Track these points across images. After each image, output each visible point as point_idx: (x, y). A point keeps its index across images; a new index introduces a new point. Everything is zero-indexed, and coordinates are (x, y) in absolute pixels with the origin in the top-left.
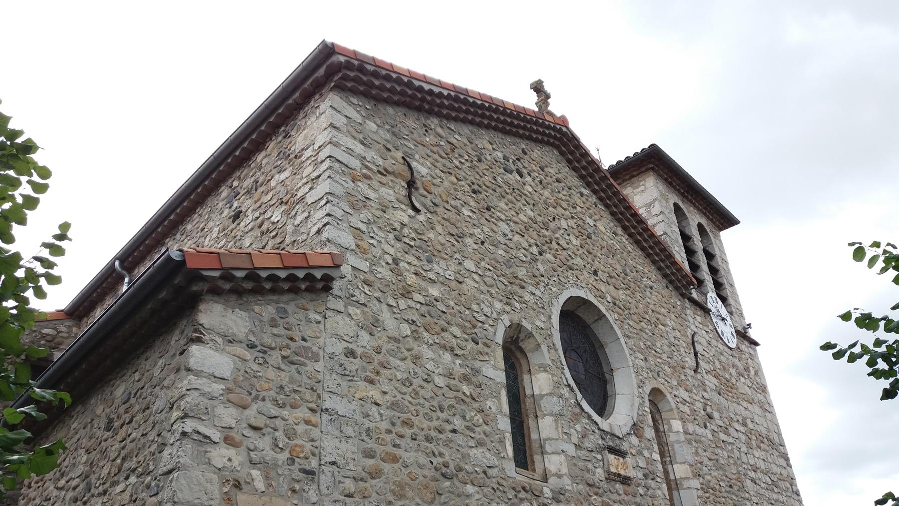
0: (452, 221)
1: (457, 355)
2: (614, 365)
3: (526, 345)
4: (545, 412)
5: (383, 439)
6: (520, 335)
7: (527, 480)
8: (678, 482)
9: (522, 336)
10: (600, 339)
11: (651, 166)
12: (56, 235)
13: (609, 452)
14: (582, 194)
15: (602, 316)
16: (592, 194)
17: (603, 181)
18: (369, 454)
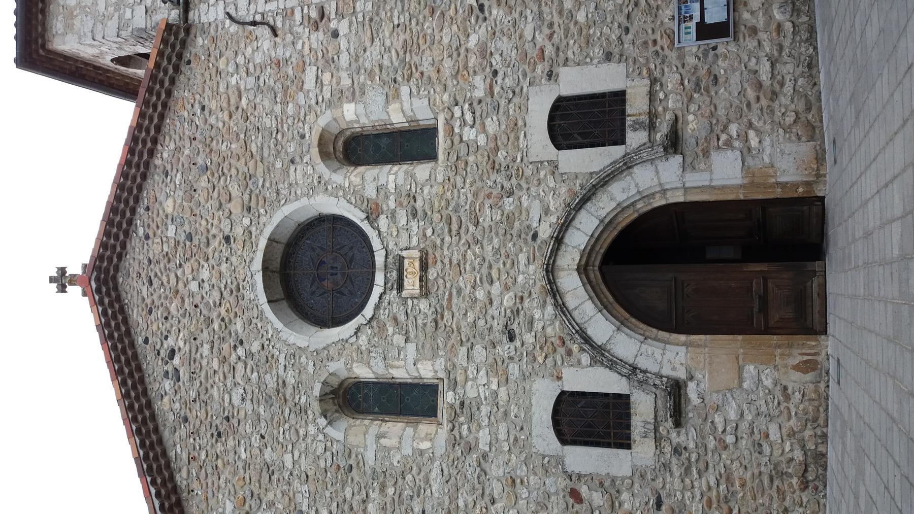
1: (367, 496)
2: (317, 214)
6: (328, 392)
9: (328, 390)
10: (294, 229)
12: (624, 102)
15: (271, 240)
16: (137, 214)
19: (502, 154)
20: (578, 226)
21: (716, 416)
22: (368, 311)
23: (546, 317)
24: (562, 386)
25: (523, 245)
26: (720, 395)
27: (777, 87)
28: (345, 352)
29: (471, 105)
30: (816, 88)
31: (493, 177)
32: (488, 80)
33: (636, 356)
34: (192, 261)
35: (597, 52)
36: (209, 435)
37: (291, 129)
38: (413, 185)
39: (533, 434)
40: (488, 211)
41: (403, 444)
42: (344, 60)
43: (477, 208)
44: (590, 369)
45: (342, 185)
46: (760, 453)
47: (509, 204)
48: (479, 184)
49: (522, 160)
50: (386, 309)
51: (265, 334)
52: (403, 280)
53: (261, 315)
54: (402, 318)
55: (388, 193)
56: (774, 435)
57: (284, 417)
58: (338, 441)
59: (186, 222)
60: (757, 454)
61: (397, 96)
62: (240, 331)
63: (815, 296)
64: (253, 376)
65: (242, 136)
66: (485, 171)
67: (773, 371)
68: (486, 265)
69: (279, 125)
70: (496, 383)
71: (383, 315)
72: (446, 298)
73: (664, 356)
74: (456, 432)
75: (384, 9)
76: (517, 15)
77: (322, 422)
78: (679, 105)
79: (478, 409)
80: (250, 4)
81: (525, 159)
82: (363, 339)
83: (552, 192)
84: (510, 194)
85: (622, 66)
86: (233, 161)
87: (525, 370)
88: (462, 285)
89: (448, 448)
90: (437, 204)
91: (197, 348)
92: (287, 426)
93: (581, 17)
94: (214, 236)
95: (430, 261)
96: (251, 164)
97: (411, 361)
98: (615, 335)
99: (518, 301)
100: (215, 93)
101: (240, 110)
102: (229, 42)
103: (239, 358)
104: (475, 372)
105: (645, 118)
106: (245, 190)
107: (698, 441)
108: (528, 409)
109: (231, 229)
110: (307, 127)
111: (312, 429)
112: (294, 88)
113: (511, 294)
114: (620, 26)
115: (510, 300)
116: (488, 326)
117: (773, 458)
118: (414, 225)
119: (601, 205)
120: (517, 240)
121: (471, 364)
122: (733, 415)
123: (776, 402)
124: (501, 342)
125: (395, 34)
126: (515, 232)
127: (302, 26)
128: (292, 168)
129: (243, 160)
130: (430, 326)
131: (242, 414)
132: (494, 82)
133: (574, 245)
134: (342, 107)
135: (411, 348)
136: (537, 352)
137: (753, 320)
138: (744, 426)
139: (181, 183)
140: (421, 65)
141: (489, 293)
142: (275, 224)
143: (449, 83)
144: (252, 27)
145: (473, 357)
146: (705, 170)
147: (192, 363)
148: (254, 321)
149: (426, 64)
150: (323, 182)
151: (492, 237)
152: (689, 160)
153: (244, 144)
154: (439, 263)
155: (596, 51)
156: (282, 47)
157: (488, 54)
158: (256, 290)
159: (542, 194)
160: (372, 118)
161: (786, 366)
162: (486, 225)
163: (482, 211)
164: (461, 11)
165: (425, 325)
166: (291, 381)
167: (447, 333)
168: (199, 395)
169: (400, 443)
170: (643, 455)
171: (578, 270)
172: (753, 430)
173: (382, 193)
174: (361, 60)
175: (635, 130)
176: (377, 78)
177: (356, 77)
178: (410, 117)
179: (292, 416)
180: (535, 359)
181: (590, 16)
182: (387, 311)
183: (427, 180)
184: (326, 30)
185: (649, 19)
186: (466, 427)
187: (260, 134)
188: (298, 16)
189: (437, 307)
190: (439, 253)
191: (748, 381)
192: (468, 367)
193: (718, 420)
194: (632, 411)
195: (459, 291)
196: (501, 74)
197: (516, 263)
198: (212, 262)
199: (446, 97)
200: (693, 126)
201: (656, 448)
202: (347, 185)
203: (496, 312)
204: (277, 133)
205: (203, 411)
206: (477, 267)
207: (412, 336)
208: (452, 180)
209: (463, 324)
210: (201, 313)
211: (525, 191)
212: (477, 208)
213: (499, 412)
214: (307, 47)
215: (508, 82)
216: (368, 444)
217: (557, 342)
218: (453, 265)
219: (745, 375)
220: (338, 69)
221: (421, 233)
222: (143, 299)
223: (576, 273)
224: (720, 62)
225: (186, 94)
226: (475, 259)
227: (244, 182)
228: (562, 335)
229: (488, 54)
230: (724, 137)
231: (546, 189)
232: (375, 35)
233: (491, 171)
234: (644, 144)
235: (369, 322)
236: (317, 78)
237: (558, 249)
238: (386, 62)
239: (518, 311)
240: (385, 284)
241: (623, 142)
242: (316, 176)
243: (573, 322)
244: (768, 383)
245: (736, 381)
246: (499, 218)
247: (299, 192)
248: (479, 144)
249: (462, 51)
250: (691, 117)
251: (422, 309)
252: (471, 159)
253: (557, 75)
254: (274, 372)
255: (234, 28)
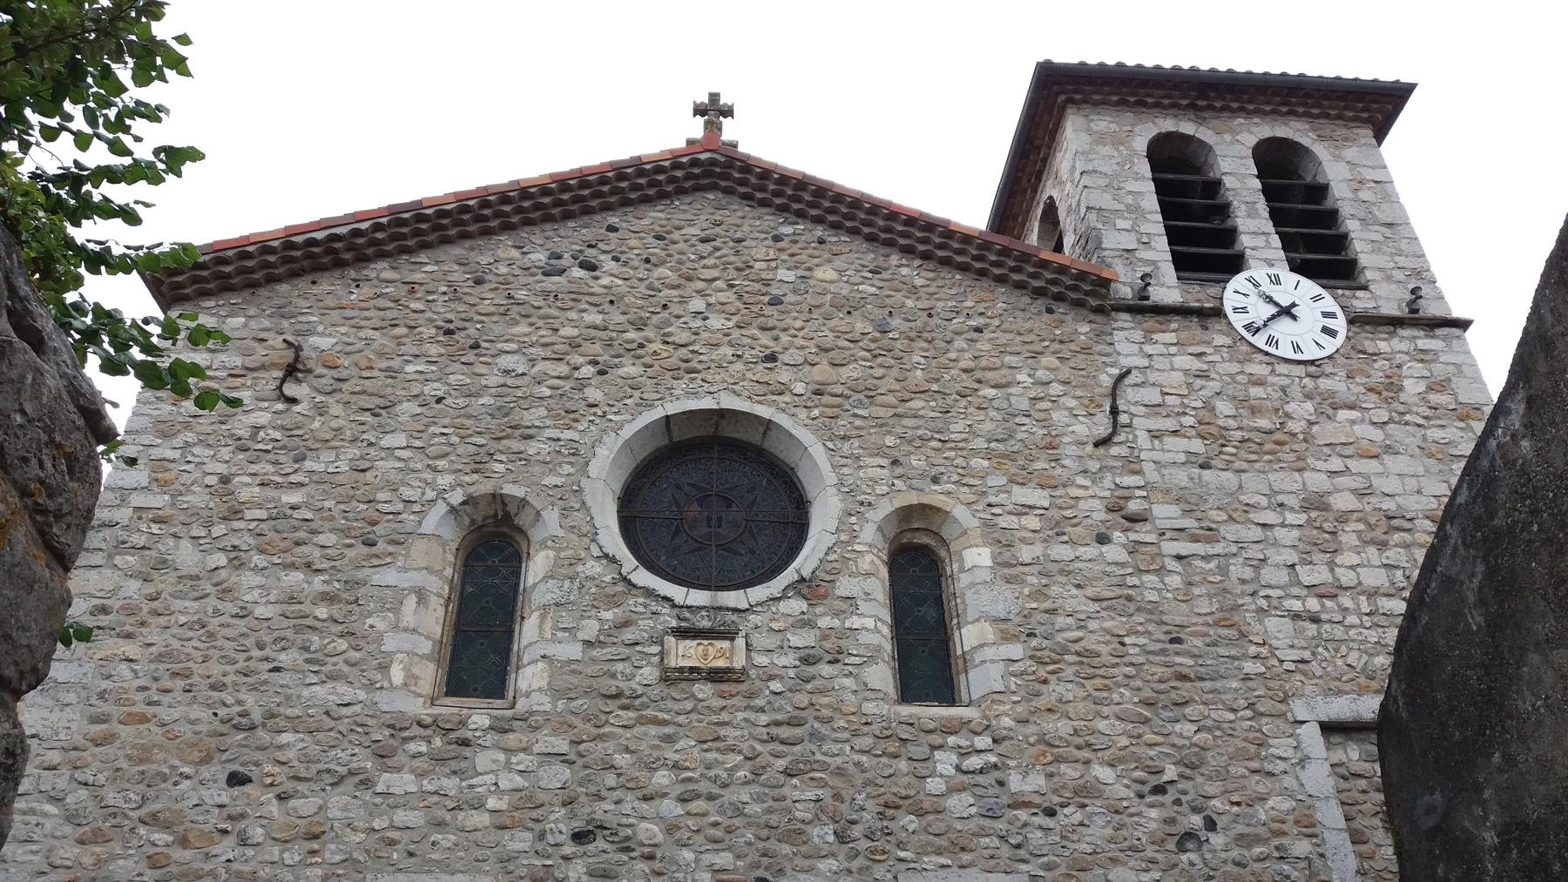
0: (370, 390)
2: (810, 497)
3: (524, 520)
5: (127, 699)
6: (508, 508)
7: (456, 710)
8: (968, 657)
9: (512, 509)
11: (1062, 98)
15: (768, 425)
17: (822, 197)
18: (97, 720)
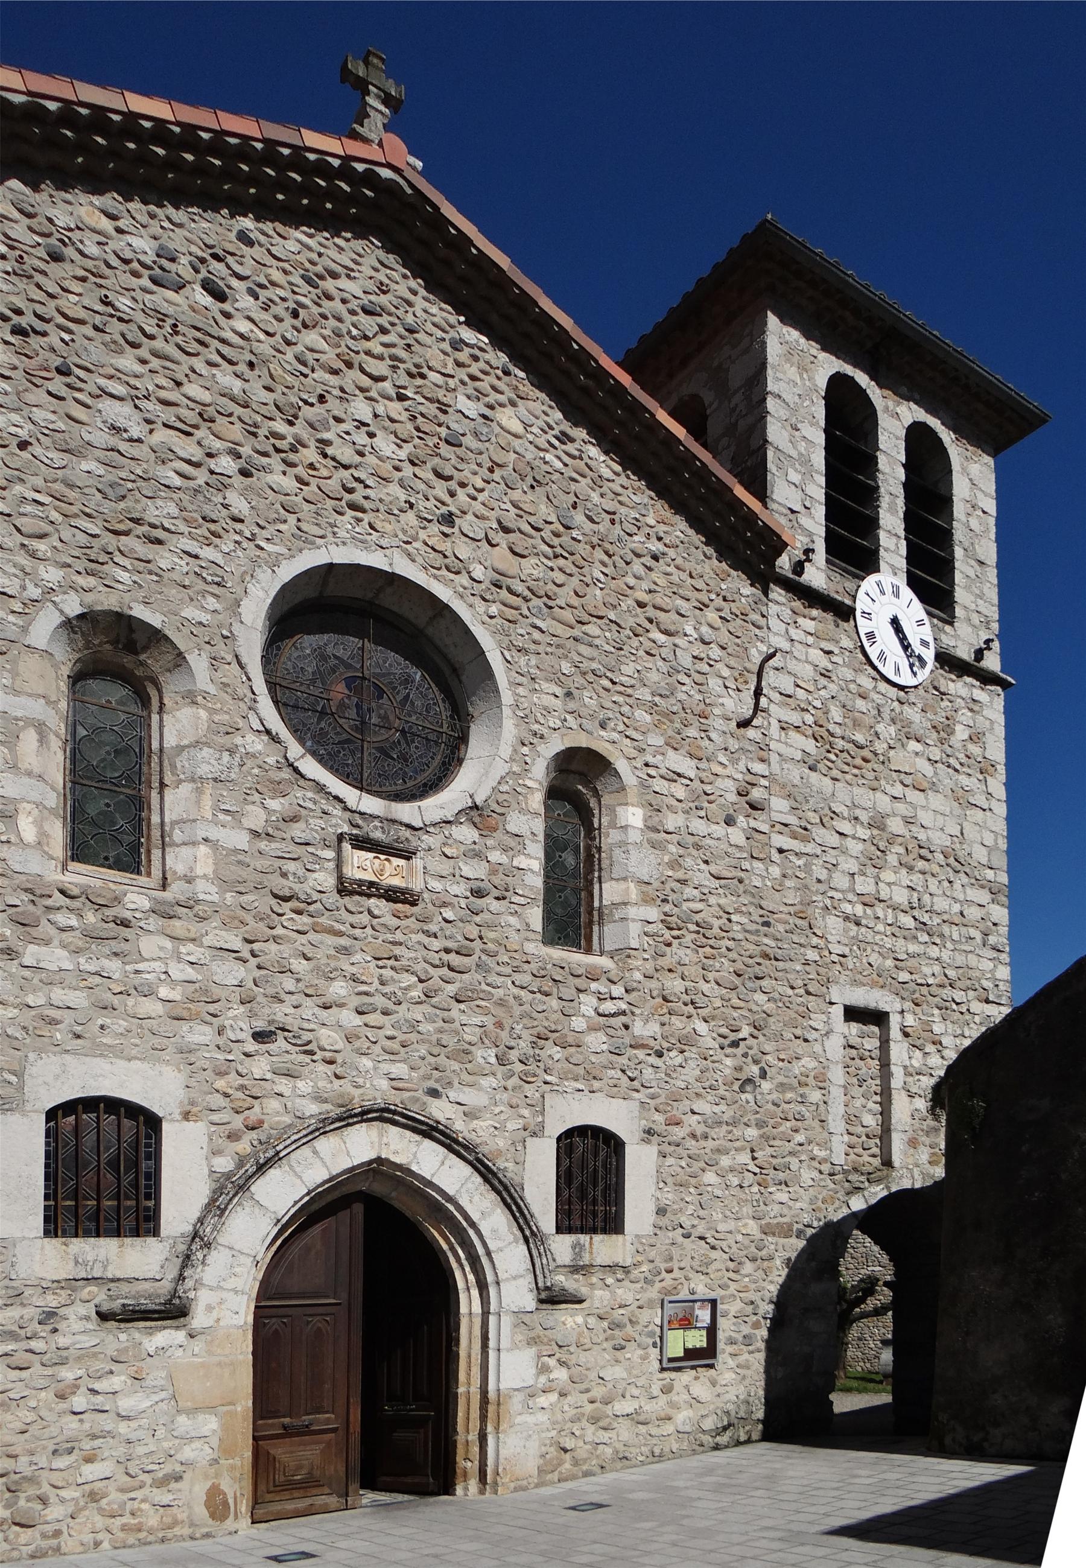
4: (182, 776)
13: (354, 847)
14: (457, 345)
19: (557, 1052)
20: (447, 1163)
21: (123, 1378)
22: (311, 767)
23: (298, 1100)
24: (172, 1120)
25: (422, 1072)
26: (163, 1382)
27: (603, 1423)
28: (228, 698)
29: (624, 1013)
30: (598, 1470)
31: (526, 1034)
32: (652, 1043)
33: (231, 1248)
34: (410, 426)
35: (668, 1196)
36: (21, 304)
37: (616, 708)
38: (522, 901)
39: (68, 1058)
40: (477, 1020)
41: (26, 780)
42: (699, 826)
43: (483, 1003)
44: (206, 1171)
45: (529, 775)
46: (55, 1452)
47: (486, 1055)
48: (517, 1011)
49: (546, 1083)
50: (315, 803)
51: (266, 534)
52: (370, 850)
53: (303, 539)
54: (298, 831)
55: (511, 853)
56: (90, 1471)
57: (76, 516)
58: (25, 630)
59: (480, 445)
60: (52, 1448)
61: (647, 900)
62: (270, 479)
63: (308, 1501)
64: (172, 474)
65: (612, 616)
66: (536, 1023)
67: (208, 1458)
68: (390, 1006)
69: (622, 689)
70: (171, 997)
71: (302, 795)
72: (335, 924)
73: (232, 1293)
74: (58, 899)
75: (751, 903)
76: (721, 1092)
77: (73, 606)
78: (597, 1304)
79: (116, 954)
80: (781, 694)
81: (547, 1087)
82: (257, 744)
83: (498, 1126)
84: (501, 1060)
85: (650, 1230)
86: (574, 582)
87: (199, 1053)
88: (358, 957)
89: (23, 878)
90: (492, 935)
91: (231, 362)
92: (55, 516)
93: (710, 1177)
94: (452, 494)
95: (399, 906)
96: (567, 615)
97: (214, 833)
98: (269, 1214)
99: (328, 1055)
100: (675, 590)
101: (647, 625)
102: (737, 640)
103: (210, 455)
104: (192, 959)
105: (586, 1260)
106: (528, 588)
107: (71, 1351)
108: (118, 1052)
109: (466, 536)
110: (615, 736)
111: (52, 575)
112: (670, 733)
113: (340, 1045)
114: (693, 1226)
115: (330, 1040)
116: (283, 996)
117: (45, 1474)
118: (460, 889)
119: (476, 1198)
120: (430, 1064)
121: (208, 952)
122: (125, 1404)
123: (150, 1467)
124: (252, 1015)
125: (722, 913)
126: (442, 1060)
127: (745, 770)
128: (559, 691)
129: (575, 601)
130: (284, 886)
131: (79, 413)
132: (650, 1052)
133: (418, 1155)
134: (637, 806)
135: (240, 840)
136: (233, 1079)
137: (270, 1418)
138: (106, 1422)
139: (546, 463)
140: (680, 944)
141: (341, 1005)
142: (472, 628)
143: (653, 984)
144: (753, 689)
145: (222, 959)
146: (513, 1341)
147: (199, 335)
148: (292, 519)
149: (681, 952)
150: (535, 741)
151: (435, 1022)
152: (527, 1318)
153: (600, 614)
154: (395, 922)
155: (670, 1196)
156: (724, 729)
157: (683, 1047)
158: (356, 547)
159: (497, 1110)
160: (617, 852)
161: (217, 1475)
162: (454, 1013)
163: (477, 1010)
164: (735, 1015)
165: (284, 875)
166: (164, 559)
167: (269, 916)
168: (120, 319)
169: (29, 774)
170: (37, 1258)
171: (379, 1160)
172: (100, 1437)
173: (512, 842)
174: (694, 852)
175: (574, 1247)
176: (670, 873)
177: (674, 838)
178: (611, 914)
179: (82, 539)
180: (221, 1074)
181: (709, 1189)
182: (310, 805)
183: (527, 925)
184: (736, 807)
185: (696, 1264)
186: (74, 922)
187: (613, 650)
188: (758, 768)
189: (318, 905)
190: (413, 926)
191: (189, 1422)
192: (201, 946)
193: (116, 1382)
194: (128, 1241)
195: (345, 951)
196: (657, 1062)
197: (392, 1057)
198: (408, 470)
199: (638, 976)
200: (569, 1319)
201: (53, 1282)
202: (529, 783)
203: (311, 1012)
204: (611, 681)
205: (82, 314)
206: (387, 989)
207: (263, 845)
208: (526, 966)
209: (286, 950)
210: (306, 402)
211: (503, 1083)
212: (483, 1003)
213: (109, 995)
214: (718, 769)
215: (648, 1072)
216: (23, 700)
217: (254, 1115)
218: (393, 948)
219: (201, 1417)
220: (688, 813)
221: (447, 900)
222: (335, 276)
223: (373, 1156)
224: (640, 1352)
225: (679, 533)
226: (400, 988)
227: (542, 593)
228: (266, 1125)
229: (683, 1047)
230: (552, 1362)
231: (503, 1117)
232: (723, 882)
233: (535, 1032)
234: (554, 1260)
235: (291, 765)
236: (679, 775)
237: (414, 1130)
238: (689, 892)
239: (311, 1053)
240: (361, 813)
241: (559, 1230)
242: (545, 731)
243: (294, 1147)
244: (188, 1453)
245: (189, 1404)
246: (467, 1038)
247: (521, 690)
248: (573, 1018)
249: (690, 1009)
250: (580, 1319)
251: (315, 875)
252: (554, 1003)
253: (648, 1142)
254: (183, 528)
255: (757, 659)
